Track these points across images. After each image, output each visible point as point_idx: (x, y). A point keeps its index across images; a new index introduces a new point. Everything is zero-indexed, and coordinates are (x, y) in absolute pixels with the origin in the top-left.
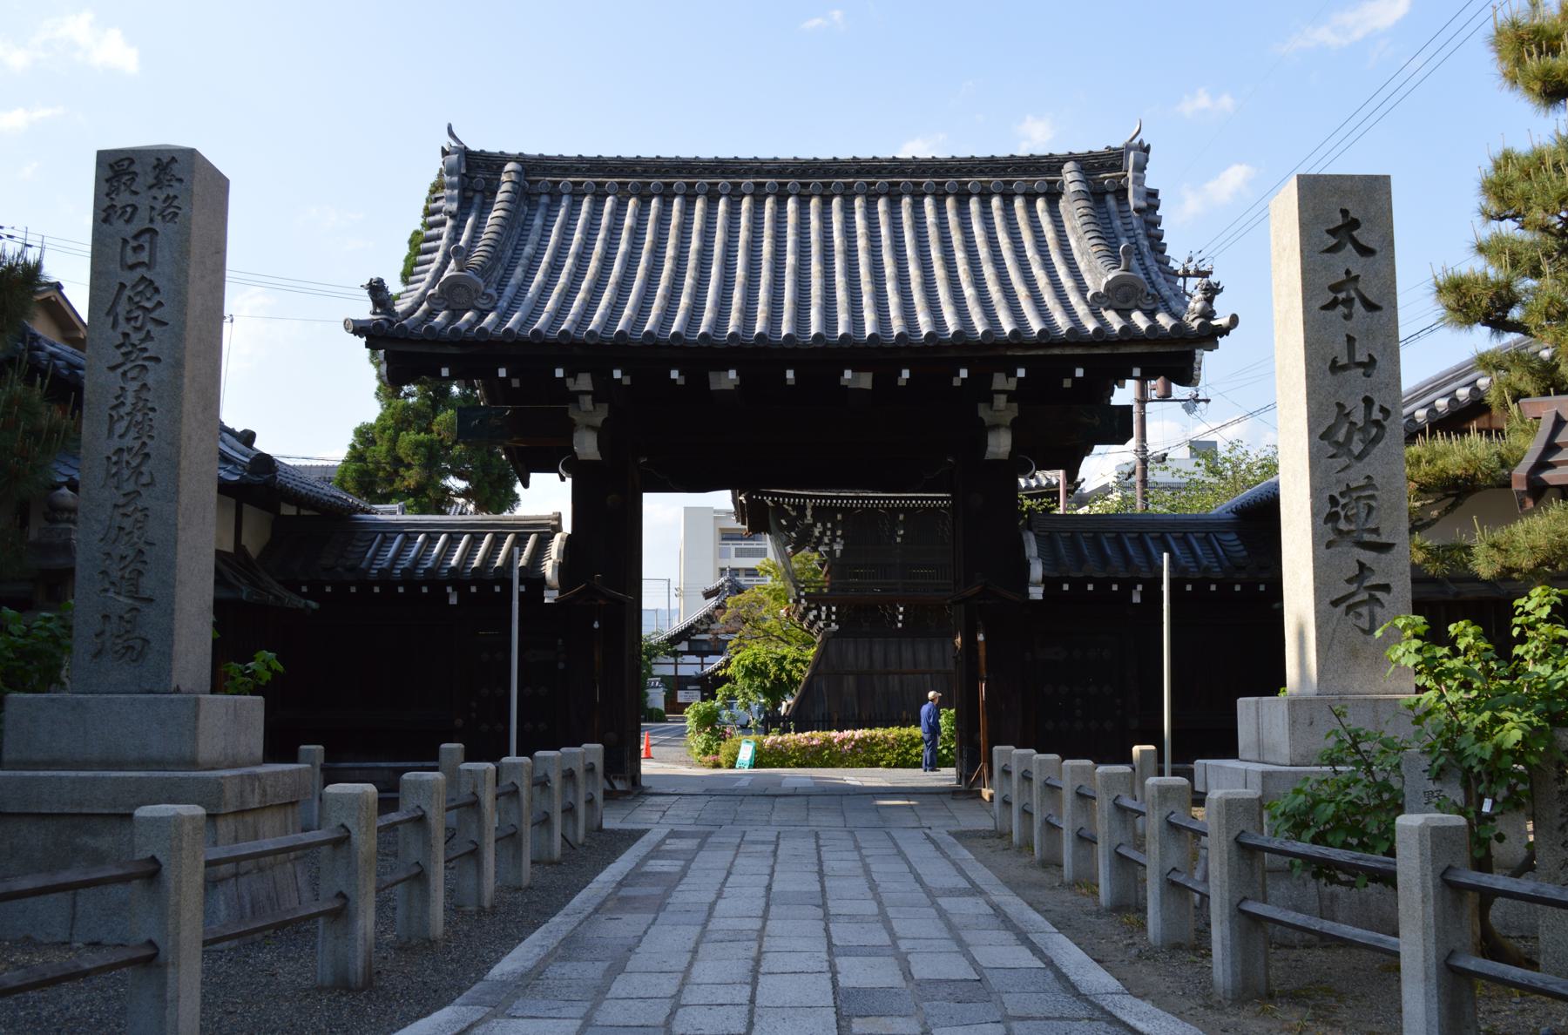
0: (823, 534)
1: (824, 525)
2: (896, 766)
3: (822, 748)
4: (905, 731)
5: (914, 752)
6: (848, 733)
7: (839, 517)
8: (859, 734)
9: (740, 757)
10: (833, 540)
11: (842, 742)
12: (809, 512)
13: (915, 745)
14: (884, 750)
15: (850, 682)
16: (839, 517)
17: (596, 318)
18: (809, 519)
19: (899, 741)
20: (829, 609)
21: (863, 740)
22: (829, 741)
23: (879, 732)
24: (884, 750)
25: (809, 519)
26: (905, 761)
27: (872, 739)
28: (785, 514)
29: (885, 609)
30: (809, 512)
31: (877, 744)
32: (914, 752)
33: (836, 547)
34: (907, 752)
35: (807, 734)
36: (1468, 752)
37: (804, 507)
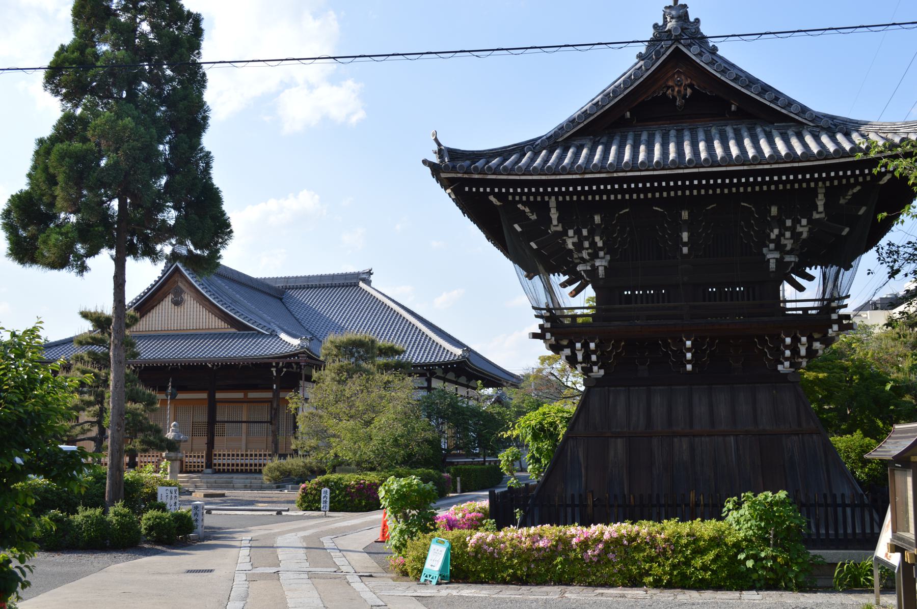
0: (579, 246)
1: (578, 233)
2: (670, 586)
3: (553, 552)
4: (685, 528)
5: (698, 562)
6: (595, 530)
7: (597, 219)
8: (610, 531)
9: (427, 565)
10: (594, 256)
11: (585, 544)
12: (554, 215)
13: (700, 552)
14: (651, 559)
15: (618, 449)
16: (597, 219)
17: (551, 161)
18: (556, 226)
19: (673, 542)
20: (585, 346)
21: (616, 542)
22: (564, 542)
23: (644, 528)
24: (651, 559)
25: (556, 226)
26: (683, 576)
27: (632, 539)
28: (521, 218)
29: (666, 345)
30: (554, 215)
31: (639, 549)
32: (698, 562)
33: (598, 263)
34: (687, 563)
35: (533, 530)
36: (331, 431)
37: (546, 207)
